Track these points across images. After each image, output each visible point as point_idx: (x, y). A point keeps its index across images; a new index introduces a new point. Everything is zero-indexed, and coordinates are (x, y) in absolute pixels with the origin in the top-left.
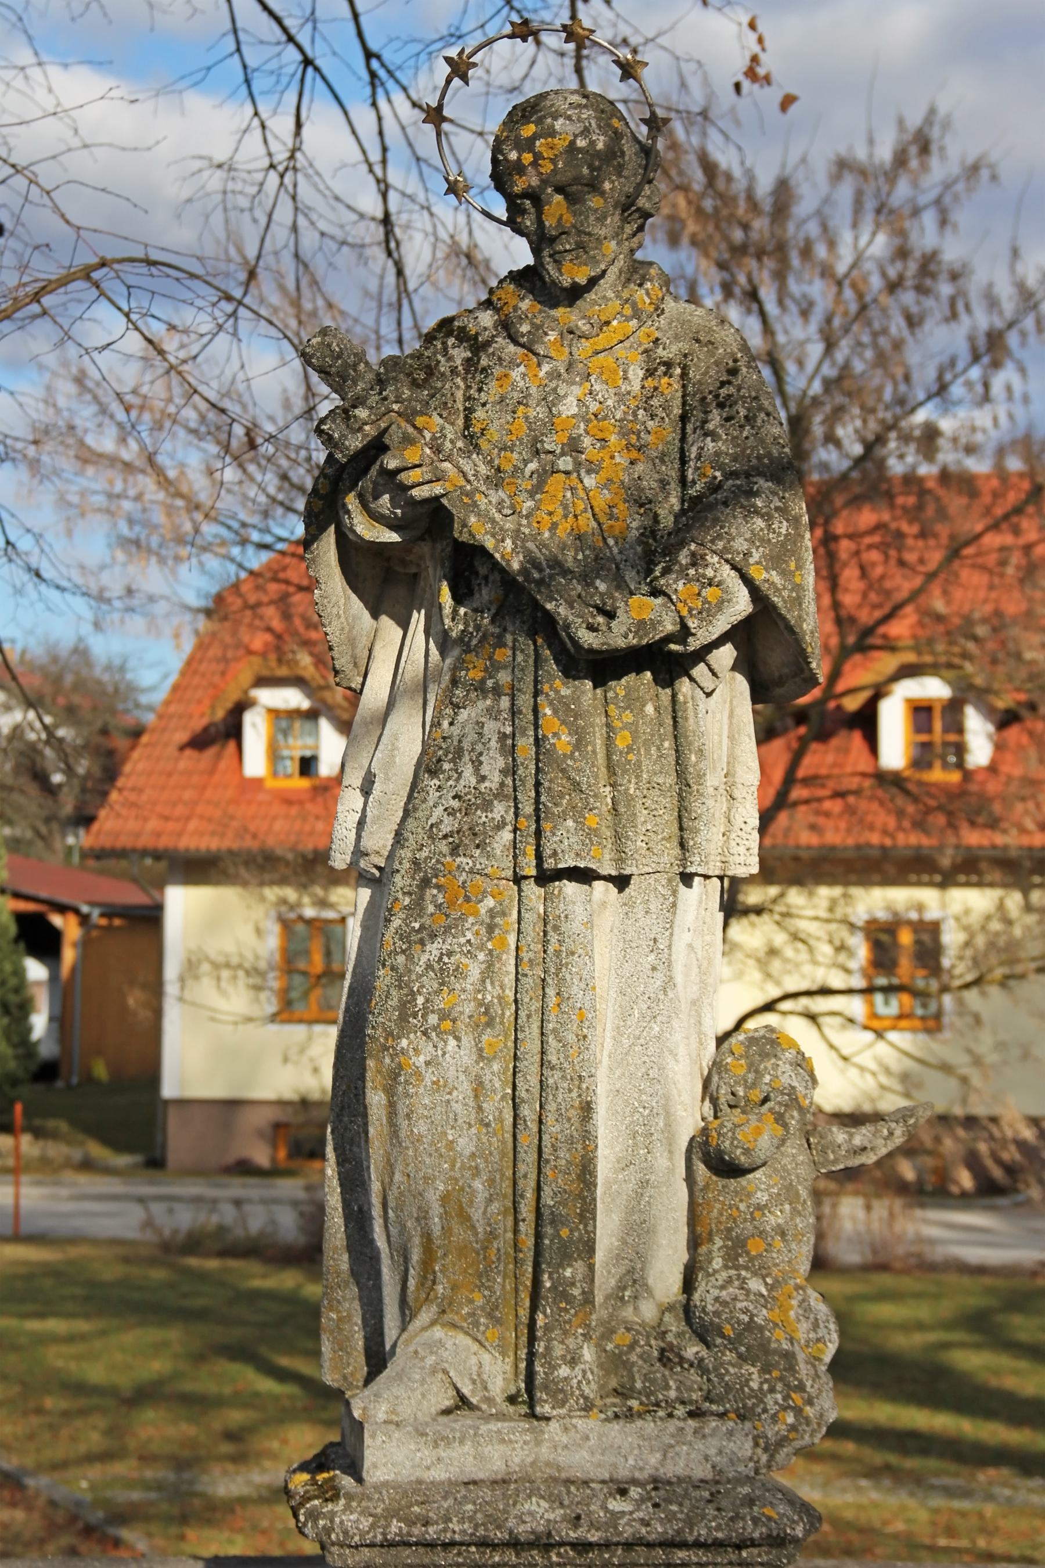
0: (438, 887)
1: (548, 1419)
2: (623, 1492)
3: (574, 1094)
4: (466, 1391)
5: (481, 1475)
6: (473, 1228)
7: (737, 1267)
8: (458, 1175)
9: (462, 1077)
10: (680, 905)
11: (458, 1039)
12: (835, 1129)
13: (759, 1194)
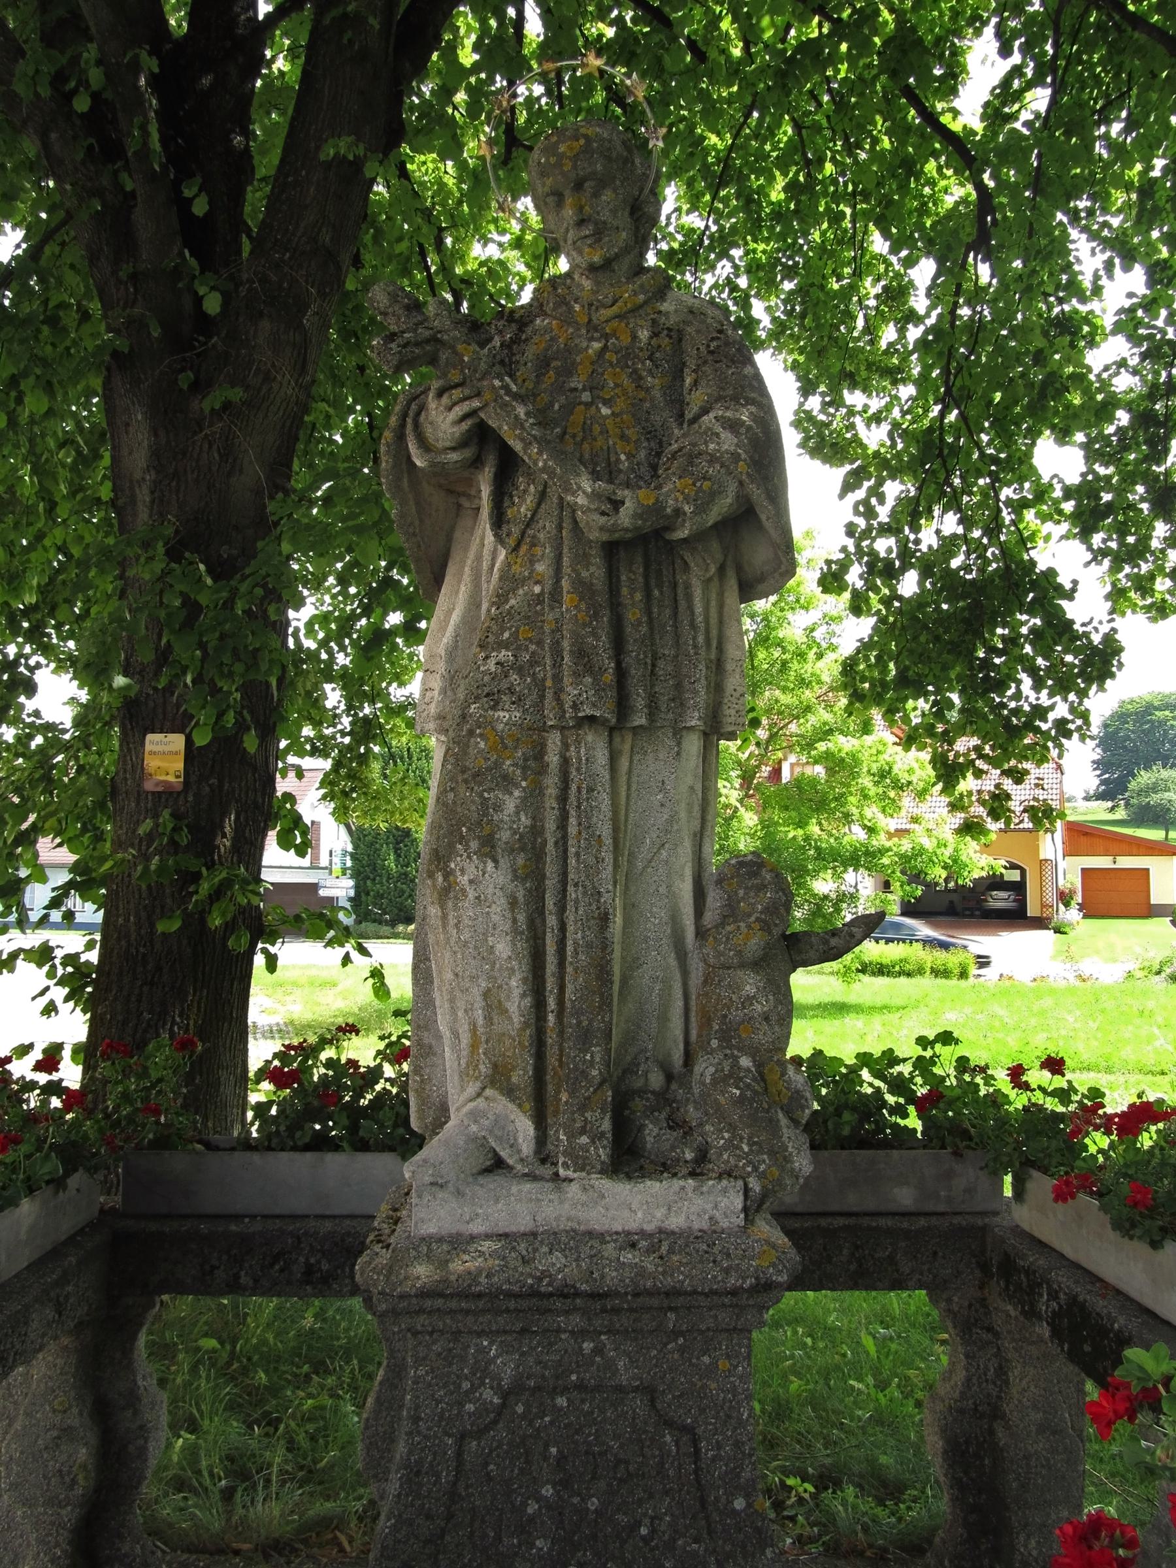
0: (481, 735)
1: (571, 1180)
2: (633, 1245)
3: (594, 907)
4: (503, 1154)
5: (514, 1229)
6: (510, 1018)
7: (730, 1047)
8: (497, 974)
9: (499, 893)
10: (684, 755)
11: (495, 861)
12: (649, 1146)
13: (748, 988)
